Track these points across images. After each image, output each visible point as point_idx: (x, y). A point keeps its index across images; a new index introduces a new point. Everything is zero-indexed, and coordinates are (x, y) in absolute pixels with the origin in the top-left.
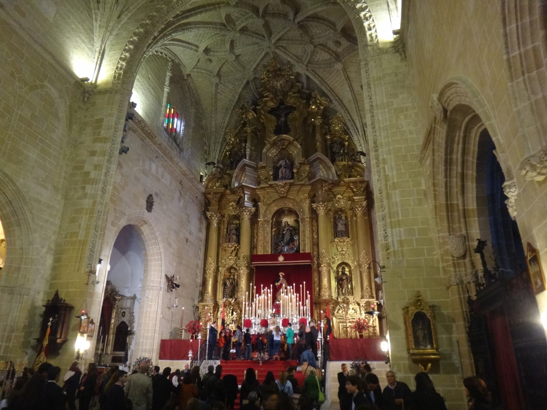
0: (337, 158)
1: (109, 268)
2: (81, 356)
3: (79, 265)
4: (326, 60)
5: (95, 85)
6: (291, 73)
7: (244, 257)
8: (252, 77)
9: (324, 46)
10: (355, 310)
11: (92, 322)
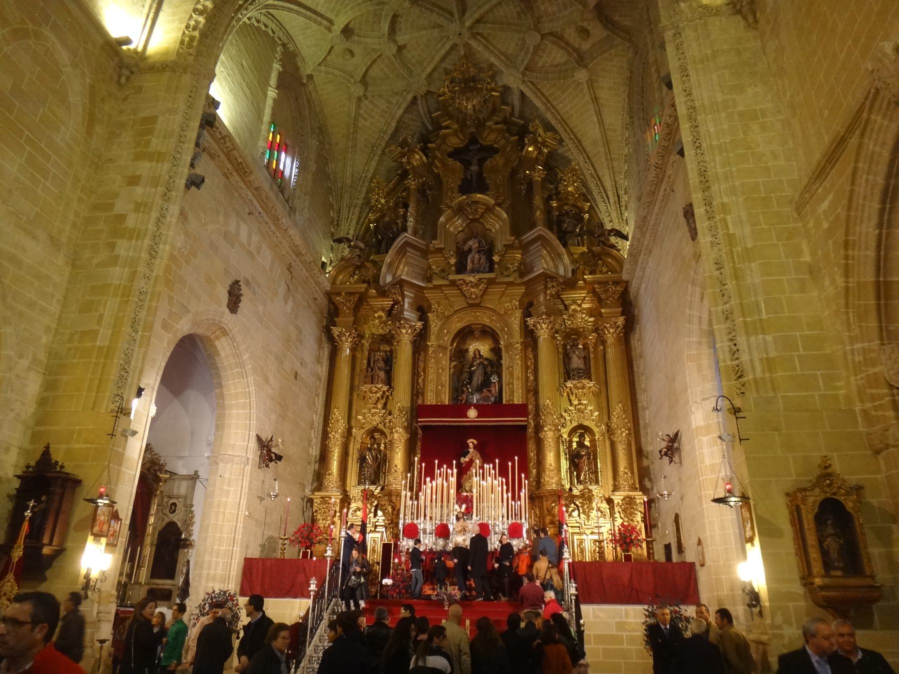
0: (570, 242)
1: (153, 410)
2: (92, 583)
3: (96, 397)
4: (557, 65)
5: (140, 57)
7: (400, 410)
8: (424, 89)
9: (557, 37)
10: (602, 512)
11: (115, 516)
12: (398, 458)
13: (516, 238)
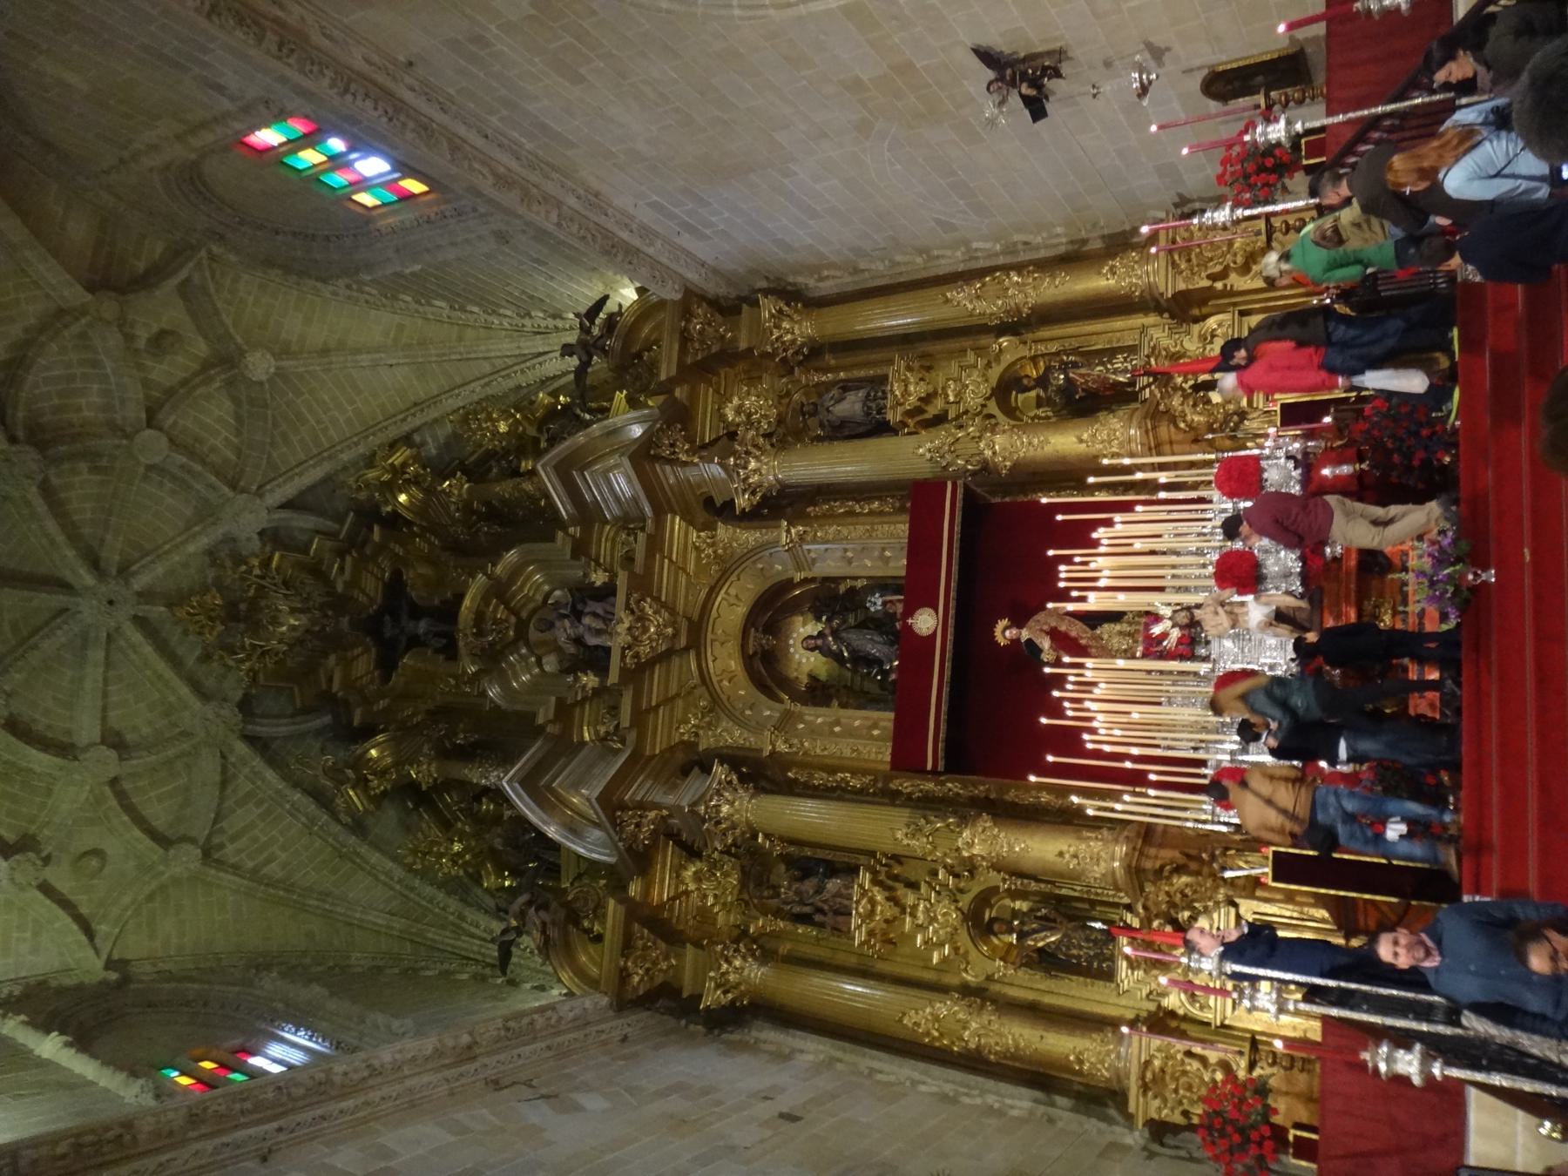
6: (255, 562)
8: (230, 713)
12: (1042, 848)
13: (564, 528)
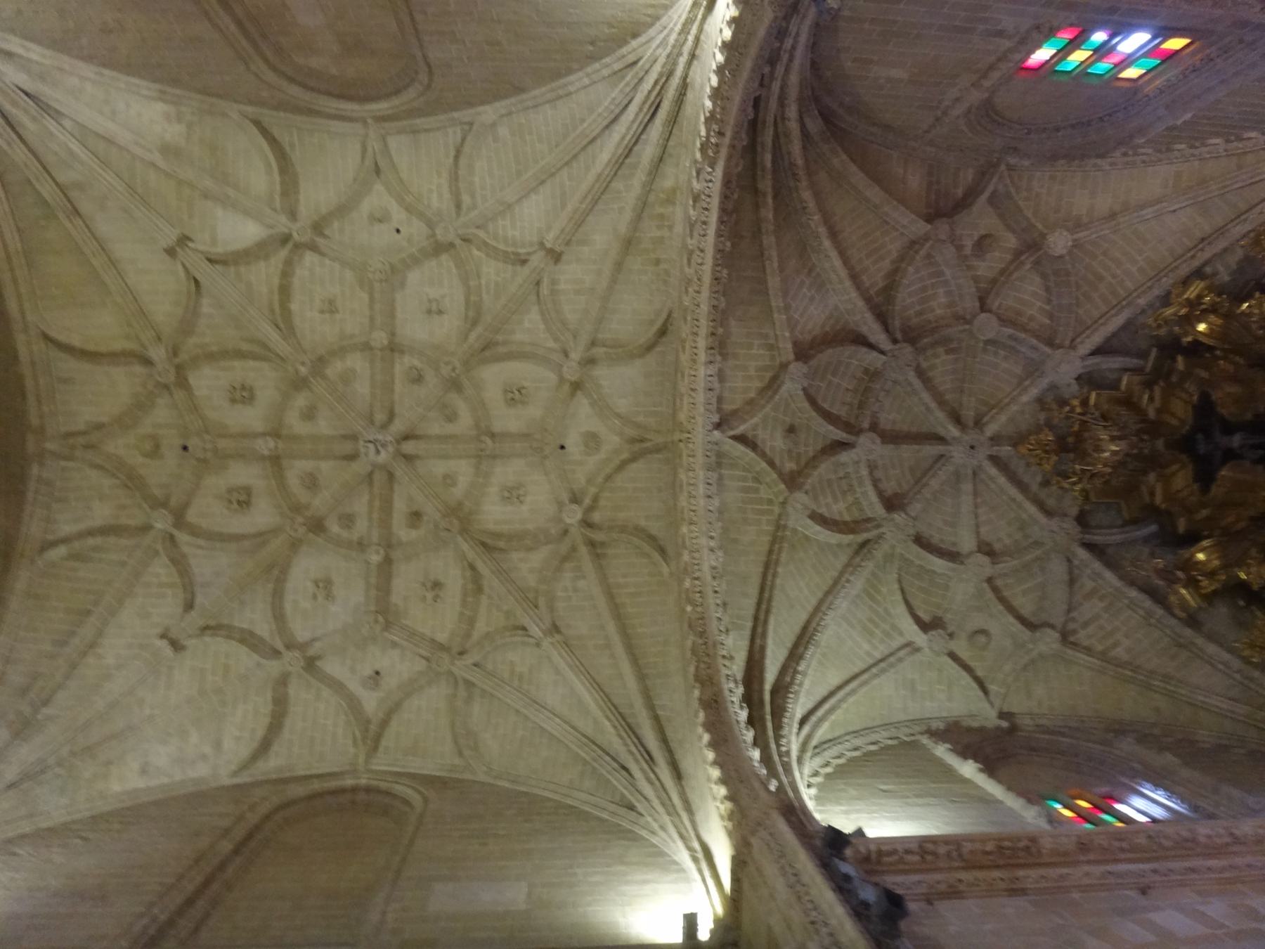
4: (1048, 289)
6: (1076, 402)
8: (1071, 526)
